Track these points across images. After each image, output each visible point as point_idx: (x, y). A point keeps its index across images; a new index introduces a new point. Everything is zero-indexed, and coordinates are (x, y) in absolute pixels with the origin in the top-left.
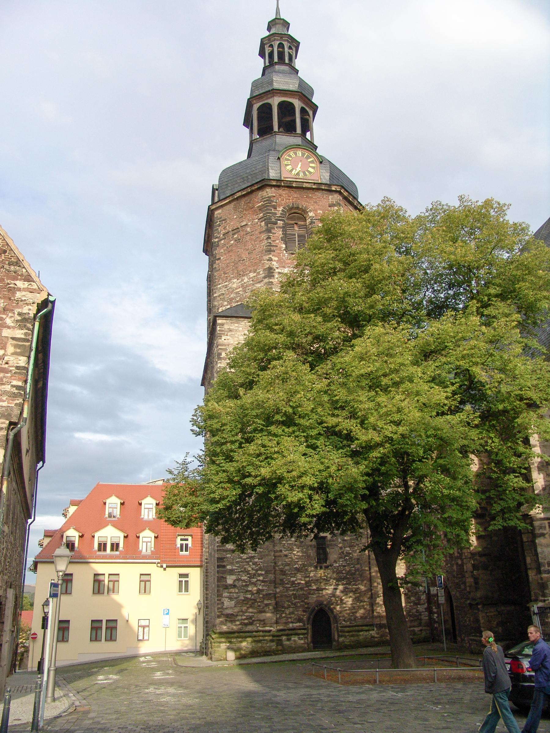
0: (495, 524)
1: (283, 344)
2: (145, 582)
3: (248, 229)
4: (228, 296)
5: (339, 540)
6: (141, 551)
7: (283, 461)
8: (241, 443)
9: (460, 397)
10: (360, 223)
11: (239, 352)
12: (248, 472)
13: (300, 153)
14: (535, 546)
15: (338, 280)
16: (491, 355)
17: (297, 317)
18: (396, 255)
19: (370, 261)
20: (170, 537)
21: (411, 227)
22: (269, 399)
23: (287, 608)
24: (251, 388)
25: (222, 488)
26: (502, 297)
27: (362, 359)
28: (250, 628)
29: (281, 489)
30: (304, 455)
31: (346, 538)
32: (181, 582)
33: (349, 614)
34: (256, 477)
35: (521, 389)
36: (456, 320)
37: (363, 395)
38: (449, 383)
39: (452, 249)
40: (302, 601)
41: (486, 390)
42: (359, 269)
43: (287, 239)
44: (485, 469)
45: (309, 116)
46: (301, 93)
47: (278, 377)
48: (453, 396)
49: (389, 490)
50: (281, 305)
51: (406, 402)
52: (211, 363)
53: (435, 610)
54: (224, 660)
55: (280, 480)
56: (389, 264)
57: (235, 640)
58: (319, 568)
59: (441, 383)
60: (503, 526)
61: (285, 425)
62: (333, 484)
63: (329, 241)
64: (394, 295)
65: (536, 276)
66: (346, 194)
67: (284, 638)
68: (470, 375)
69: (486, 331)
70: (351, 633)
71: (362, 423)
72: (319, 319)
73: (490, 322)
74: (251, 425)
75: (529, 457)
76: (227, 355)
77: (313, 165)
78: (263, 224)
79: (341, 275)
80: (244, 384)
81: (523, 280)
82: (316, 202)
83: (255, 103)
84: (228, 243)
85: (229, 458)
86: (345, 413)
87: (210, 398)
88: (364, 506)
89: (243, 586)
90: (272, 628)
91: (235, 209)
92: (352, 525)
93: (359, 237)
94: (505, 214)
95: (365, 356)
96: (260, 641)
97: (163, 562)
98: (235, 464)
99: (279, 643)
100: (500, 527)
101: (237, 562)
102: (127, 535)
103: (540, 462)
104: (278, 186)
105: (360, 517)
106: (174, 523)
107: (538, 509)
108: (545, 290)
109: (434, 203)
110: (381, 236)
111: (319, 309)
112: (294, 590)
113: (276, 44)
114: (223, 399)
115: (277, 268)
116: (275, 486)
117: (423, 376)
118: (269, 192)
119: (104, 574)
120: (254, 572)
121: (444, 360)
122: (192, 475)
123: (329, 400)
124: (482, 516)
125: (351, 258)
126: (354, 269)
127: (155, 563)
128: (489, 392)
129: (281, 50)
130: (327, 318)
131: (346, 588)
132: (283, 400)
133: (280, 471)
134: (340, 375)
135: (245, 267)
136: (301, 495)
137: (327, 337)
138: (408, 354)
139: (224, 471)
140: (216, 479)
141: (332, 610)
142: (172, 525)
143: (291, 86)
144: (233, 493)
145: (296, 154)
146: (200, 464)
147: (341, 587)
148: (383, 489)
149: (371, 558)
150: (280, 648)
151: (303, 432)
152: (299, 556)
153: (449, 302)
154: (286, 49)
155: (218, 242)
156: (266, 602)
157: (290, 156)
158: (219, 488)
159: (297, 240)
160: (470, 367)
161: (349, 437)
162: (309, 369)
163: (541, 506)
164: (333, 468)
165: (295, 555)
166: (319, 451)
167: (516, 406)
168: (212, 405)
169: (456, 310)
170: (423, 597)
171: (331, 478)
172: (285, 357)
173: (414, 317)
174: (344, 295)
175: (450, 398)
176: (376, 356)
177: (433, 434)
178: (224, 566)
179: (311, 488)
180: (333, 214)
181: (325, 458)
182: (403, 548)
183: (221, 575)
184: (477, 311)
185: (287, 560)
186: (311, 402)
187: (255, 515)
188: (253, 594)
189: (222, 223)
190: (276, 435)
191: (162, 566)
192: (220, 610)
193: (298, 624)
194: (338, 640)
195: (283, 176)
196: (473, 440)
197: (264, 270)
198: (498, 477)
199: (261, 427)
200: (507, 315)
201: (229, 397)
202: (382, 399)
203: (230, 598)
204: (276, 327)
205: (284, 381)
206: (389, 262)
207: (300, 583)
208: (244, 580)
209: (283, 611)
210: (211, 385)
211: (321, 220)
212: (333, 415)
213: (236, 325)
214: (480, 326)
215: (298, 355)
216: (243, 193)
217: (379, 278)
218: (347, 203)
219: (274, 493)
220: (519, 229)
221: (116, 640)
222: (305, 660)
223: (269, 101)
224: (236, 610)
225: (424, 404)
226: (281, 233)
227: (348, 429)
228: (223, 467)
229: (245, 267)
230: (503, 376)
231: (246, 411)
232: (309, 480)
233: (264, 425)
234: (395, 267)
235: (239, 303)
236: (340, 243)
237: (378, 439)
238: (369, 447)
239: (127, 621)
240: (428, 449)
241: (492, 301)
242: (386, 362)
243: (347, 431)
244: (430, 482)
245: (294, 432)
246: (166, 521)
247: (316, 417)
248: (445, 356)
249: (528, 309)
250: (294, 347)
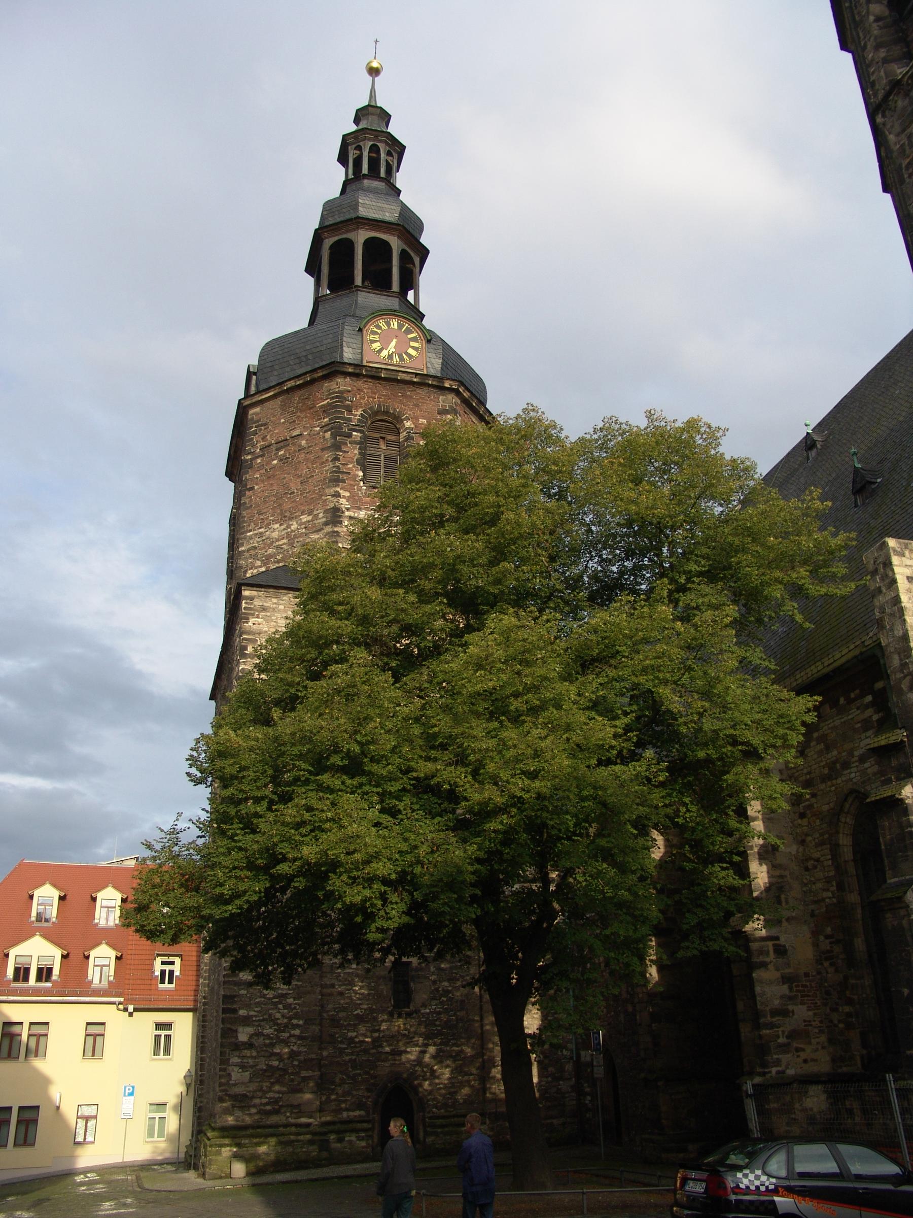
0: (688, 948)
1: (350, 638)
2: (94, 1036)
3: (303, 443)
4: (263, 551)
5: (432, 969)
6: (91, 982)
7: (340, 834)
8: (271, 802)
9: (636, 736)
10: (487, 443)
11: (275, 646)
12: (281, 853)
13: (396, 324)
14: (751, 983)
15: (446, 535)
16: (689, 669)
17: (375, 593)
18: (542, 498)
19: (499, 506)
20: (143, 957)
21: (569, 455)
22: (322, 728)
23: (340, 1085)
24: (293, 709)
25: (236, 877)
26: (710, 576)
27: (479, 667)
28: (274, 1119)
29: (335, 883)
30: (377, 825)
31: (443, 966)
32: (158, 1037)
33: (444, 1096)
34: (295, 860)
35: (734, 727)
36: (635, 609)
37: (479, 728)
38: (620, 712)
39: (633, 495)
41: (679, 725)
42: (481, 519)
43: (363, 463)
44: (674, 855)
45: (414, 264)
46: (403, 226)
47: (338, 692)
48: (625, 734)
49: (517, 886)
50: (349, 572)
51: (548, 742)
52: (229, 663)
53: (587, 1090)
54: (226, 1177)
55: (334, 866)
56: (531, 513)
57: (247, 1141)
58: (396, 1016)
59: (607, 712)
60: (701, 951)
61: (346, 774)
62: (423, 875)
63: (434, 470)
64: (536, 564)
65: (763, 545)
66: (466, 395)
67: (332, 1137)
68: (654, 701)
69: (683, 629)
70: (446, 1129)
71: (475, 773)
72: (413, 598)
73: (689, 616)
74: (289, 771)
75: (745, 838)
76: (256, 651)
77: (416, 345)
78: (328, 435)
79: (451, 527)
80: (282, 701)
81: (744, 550)
82: (417, 406)
83: (326, 238)
84: (269, 463)
85: (250, 827)
86: (447, 756)
87: (223, 722)
88: (474, 912)
89: (265, 1045)
90: (311, 1120)
91: (283, 407)
92: (455, 942)
93: (484, 466)
94: (719, 444)
95: (484, 662)
96: (291, 1143)
97: (128, 1001)
98: (258, 837)
99: (324, 1145)
100: (696, 952)
102: (68, 954)
103: (762, 846)
104: (357, 376)
105: (468, 930)
106: (152, 934)
107: (757, 923)
108: (777, 568)
109: (606, 420)
110: (520, 466)
111: (413, 581)
112: (352, 1054)
113: (367, 146)
114: (244, 724)
115: (348, 509)
116: (325, 877)
117: (578, 698)
118: (342, 384)
119: (21, 1023)
120: (286, 1021)
121: (612, 673)
122: (186, 852)
123: (422, 733)
124: (667, 933)
125: (469, 500)
126: (473, 518)
127: (114, 1003)
128: (683, 729)
129: (374, 155)
130: (424, 598)
131: (439, 1051)
132: (345, 731)
133: (335, 852)
134: (443, 692)
135: (294, 505)
136: (367, 893)
137: (423, 629)
138: (554, 662)
139: (240, 849)
140: (227, 861)
141: (415, 1089)
142: (148, 938)
143: (387, 214)
144: (257, 886)
145: (388, 324)
146: (200, 833)
147: (432, 1049)
148: (507, 884)
149: (484, 1000)
150: (325, 1154)
151: (377, 786)
152: (363, 994)
153: (626, 580)
154: (383, 155)
155: (251, 460)
156: (304, 1074)
157: (379, 327)
158: (230, 877)
159: (382, 465)
160: (655, 686)
161: (453, 796)
162: (391, 680)
163: (762, 917)
164: (423, 850)
165: (356, 992)
166: (402, 820)
167: (726, 754)
168: (225, 734)
169: (635, 592)
170: (569, 1067)
171: (419, 866)
172: (351, 660)
173: (567, 603)
174: (455, 561)
175: (620, 736)
176: (502, 663)
177: (591, 796)
178: (235, 1011)
179: (386, 881)
180: (443, 426)
181: (410, 831)
182: (536, 983)
183: (229, 1026)
184: (669, 596)
185: (342, 1001)
186: (391, 736)
187: (292, 923)
188: (281, 1060)
190: (330, 790)
191: (126, 1010)
192: (223, 1088)
193: (357, 1113)
194: (425, 1140)
195: (365, 359)
196: (656, 807)
197: (326, 512)
198: (695, 869)
199: (307, 776)
200: (716, 607)
201: (255, 722)
202: (510, 734)
203: (243, 1067)
204: (340, 608)
205: (349, 698)
206: (530, 510)
207: (364, 1041)
208: (268, 1035)
209: (333, 1090)
210: (226, 700)
211: (424, 436)
212: (428, 759)
213: (275, 600)
214: (674, 620)
215: (374, 655)
216: (298, 383)
217: (512, 536)
218: (468, 410)
219: (324, 888)
220: (741, 469)
221: (33, 1144)
222: (366, 1176)
223: (350, 236)
225: (578, 745)
226: (356, 452)
227: (452, 782)
228: (240, 841)
229: (294, 505)
230: (707, 705)
231: (283, 748)
232: (382, 868)
233: (310, 772)
234: (540, 519)
235: (281, 564)
236: (452, 474)
237: (499, 800)
238: (486, 812)
239: (58, 1108)
240: (583, 819)
241: (693, 582)
242: (519, 673)
243: (450, 785)
244: (584, 874)
245: (361, 785)
246: (137, 931)
247: (398, 761)
248: (616, 668)
249: (749, 598)
250: (368, 643)
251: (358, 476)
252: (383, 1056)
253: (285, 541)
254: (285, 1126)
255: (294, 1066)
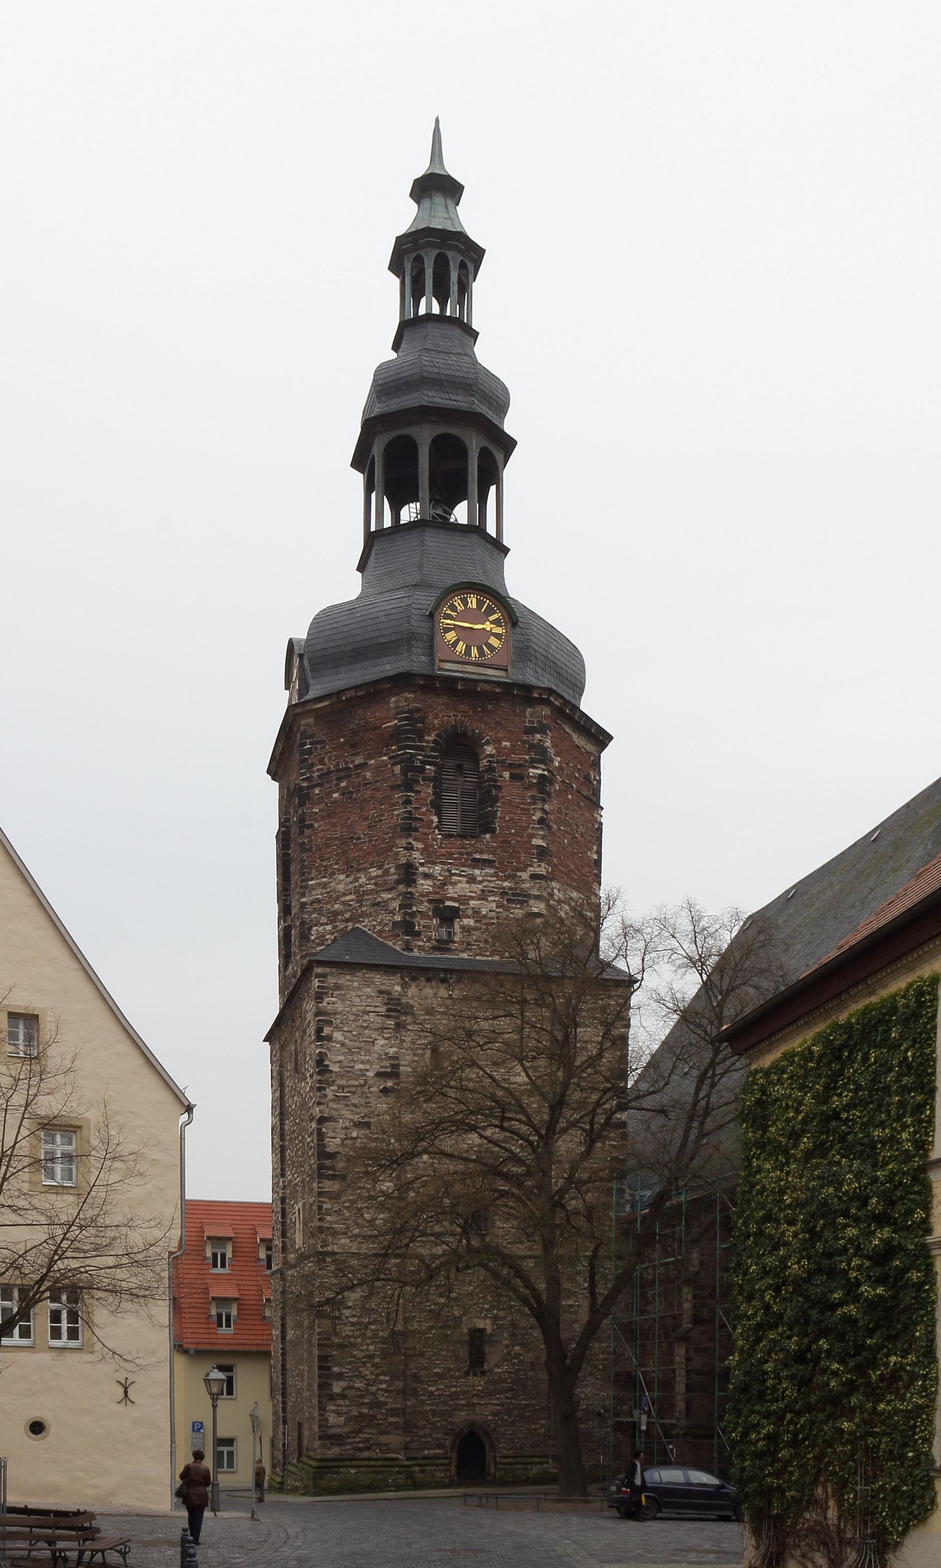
3: (368, 775)
13: (474, 600)
28: (366, 1454)
40: (446, 1420)
58: (471, 1374)
67: (417, 1469)
77: (499, 630)
78: (397, 769)
89: (357, 1396)
101: (350, 1362)
112: (432, 1404)
115: (422, 864)
155: (308, 788)
156: (391, 1419)
157: (453, 608)
178: (329, 1368)
189: (316, 749)
193: (437, 1451)
197: (398, 867)
203: (339, 1414)
213: (349, 977)
216: (359, 694)
223: (411, 431)
224: (346, 1429)
226: (430, 791)
251: (432, 821)
252: (459, 1408)
253: (353, 897)
254: (376, 1460)
255: (382, 1414)
